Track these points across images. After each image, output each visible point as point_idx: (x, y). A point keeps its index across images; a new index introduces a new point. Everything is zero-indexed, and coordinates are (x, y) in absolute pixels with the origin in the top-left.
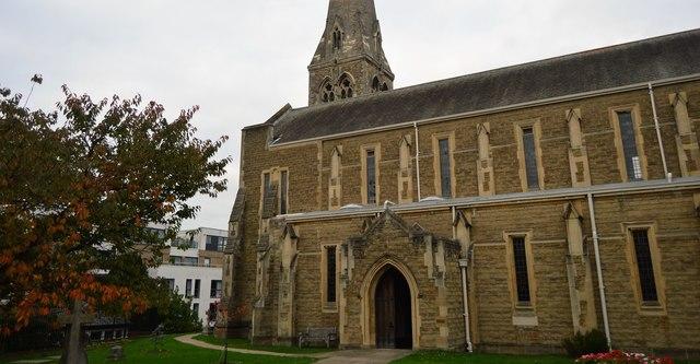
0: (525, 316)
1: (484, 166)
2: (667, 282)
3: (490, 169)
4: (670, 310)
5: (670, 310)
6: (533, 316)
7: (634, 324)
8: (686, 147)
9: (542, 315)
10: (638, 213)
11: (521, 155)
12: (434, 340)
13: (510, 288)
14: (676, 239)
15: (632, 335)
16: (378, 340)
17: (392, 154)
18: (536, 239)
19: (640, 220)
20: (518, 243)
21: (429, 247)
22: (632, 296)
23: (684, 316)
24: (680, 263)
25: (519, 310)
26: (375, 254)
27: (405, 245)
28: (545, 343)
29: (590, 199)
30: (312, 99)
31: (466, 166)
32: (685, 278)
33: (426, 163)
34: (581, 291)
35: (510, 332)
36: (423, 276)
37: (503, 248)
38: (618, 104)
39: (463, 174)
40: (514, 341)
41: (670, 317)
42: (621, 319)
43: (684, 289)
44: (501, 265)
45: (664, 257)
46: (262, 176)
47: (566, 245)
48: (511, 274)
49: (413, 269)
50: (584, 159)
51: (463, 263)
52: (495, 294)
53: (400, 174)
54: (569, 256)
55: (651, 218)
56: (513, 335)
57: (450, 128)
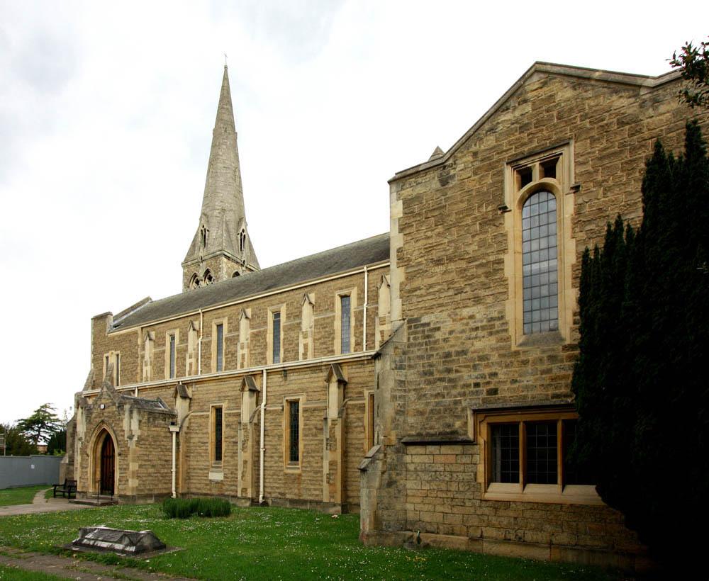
1: (242, 348)
2: (305, 445)
5: (304, 469)
6: (221, 472)
7: (280, 480)
8: (382, 328)
9: (227, 471)
12: (125, 489)
13: (209, 451)
15: (277, 488)
18: (229, 410)
19: (296, 392)
20: (219, 411)
21: (127, 414)
22: (281, 457)
23: (311, 474)
24: (314, 430)
26: (97, 420)
27: (113, 413)
28: (227, 493)
29: (265, 374)
30: (187, 286)
31: (232, 348)
32: (316, 442)
33: (207, 345)
34: (245, 452)
36: (121, 438)
37: (208, 417)
38: (341, 289)
39: (230, 356)
40: (209, 492)
41: (303, 475)
42: (273, 475)
43: (314, 451)
44: (205, 431)
45: (306, 425)
46: (105, 359)
47: (239, 415)
48: (211, 438)
49: (116, 433)
50: (310, 341)
53: (188, 356)
55: (303, 391)
57: (225, 314)
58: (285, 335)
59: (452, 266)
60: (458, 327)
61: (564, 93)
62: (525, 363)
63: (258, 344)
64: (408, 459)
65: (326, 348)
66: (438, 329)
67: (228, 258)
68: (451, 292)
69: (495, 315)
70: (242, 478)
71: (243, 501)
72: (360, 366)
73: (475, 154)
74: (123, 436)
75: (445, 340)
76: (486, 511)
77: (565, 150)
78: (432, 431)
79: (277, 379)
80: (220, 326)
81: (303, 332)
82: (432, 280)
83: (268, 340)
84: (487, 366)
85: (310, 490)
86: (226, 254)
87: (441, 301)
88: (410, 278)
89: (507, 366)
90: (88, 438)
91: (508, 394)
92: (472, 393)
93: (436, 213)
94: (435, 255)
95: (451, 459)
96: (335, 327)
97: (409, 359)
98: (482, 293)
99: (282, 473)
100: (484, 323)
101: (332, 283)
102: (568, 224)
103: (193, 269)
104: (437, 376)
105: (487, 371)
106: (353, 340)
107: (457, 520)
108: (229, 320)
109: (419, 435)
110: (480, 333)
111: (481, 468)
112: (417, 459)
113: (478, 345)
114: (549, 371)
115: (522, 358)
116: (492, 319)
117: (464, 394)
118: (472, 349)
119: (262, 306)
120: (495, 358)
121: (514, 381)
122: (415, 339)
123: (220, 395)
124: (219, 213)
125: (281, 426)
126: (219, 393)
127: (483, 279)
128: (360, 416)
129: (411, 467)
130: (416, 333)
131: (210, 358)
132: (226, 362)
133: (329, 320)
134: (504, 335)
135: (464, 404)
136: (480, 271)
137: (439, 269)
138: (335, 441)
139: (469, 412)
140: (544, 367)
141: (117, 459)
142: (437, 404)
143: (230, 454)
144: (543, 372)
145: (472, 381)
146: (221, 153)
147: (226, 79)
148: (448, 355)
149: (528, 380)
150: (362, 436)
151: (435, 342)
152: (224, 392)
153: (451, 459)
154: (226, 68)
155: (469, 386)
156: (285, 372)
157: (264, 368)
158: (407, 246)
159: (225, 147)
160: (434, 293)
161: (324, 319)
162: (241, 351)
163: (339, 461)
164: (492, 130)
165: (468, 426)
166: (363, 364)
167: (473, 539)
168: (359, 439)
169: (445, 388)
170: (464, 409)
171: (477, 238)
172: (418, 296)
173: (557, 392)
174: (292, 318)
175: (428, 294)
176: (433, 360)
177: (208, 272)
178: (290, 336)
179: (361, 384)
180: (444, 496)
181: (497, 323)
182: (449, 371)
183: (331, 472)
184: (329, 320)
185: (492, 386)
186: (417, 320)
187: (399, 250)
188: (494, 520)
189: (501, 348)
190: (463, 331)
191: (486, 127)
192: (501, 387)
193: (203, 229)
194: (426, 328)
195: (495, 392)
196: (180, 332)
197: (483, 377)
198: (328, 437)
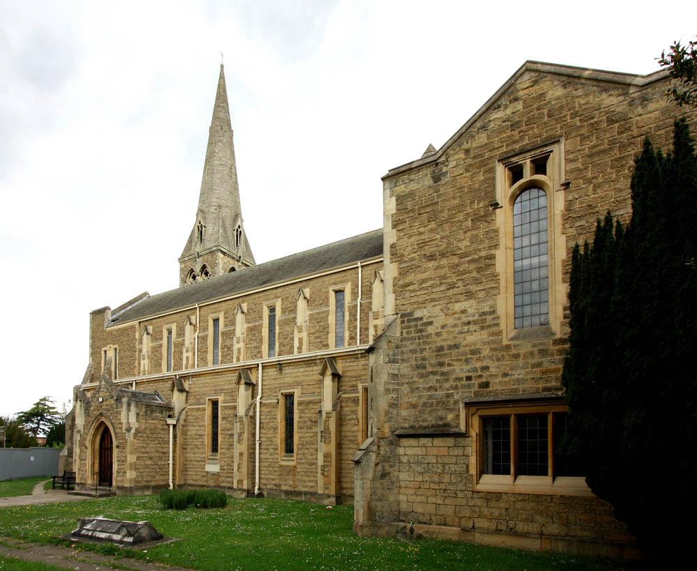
0: (213, 464)
1: (300, 331)
2: (300, 438)
3: (241, 345)
4: (298, 461)
5: (298, 461)
7: (275, 471)
9: (223, 463)
10: (289, 380)
11: (332, 319)
12: (123, 481)
13: (206, 443)
14: (310, 402)
15: (273, 479)
16: (107, 481)
17: (291, 309)
18: (225, 403)
20: (215, 404)
21: (125, 407)
23: (306, 466)
25: (211, 459)
26: (95, 412)
27: (112, 405)
28: (222, 485)
29: (260, 368)
31: (228, 342)
32: (311, 435)
33: (203, 339)
34: (241, 444)
35: (203, 476)
37: (204, 410)
39: (226, 350)
40: (205, 484)
41: (298, 466)
42: (268, 467)
43: (308, 444)
46: (103, 353)
47: (235, 408)
50: (304, 335)
51: (171, 421)
52: (196, 446)
53: (184, 350)
54: (236, 416)
55: (298, 384)
56: (205, 479)
57: (348, 278)
58: (280, 329)
59: (444, 261)
60: (451, 321)
61: (555, 92)
62: (516, 356)
63: (254, 338)
64: (401, 451)
65: (321, 342)
66: (431, 323)
67: (224, 253)
68: (443, 287)
69: (487, 309)
70: (238, 470)
71: (239, 492)
72: (354, 360)
73: (467, 151)
74: (121, 428)
75: (438, 334)
76: (478, 502)
77: (555, 148)
78: (425, 424)
79: (272, 372)
80: (216, 321)
81: (298, 327)
82: (425, 276)
83: (263, 334)
84: (478, 360)
85: (304, 482)
86: (222, 249)
87: (433, 296)
88: (403, 273)
89: (498, 360)
90: (86, 430)
91: (499, 388)
92: (464, 386)
93: (429, 209)
94: (428, 250)
95: (444, 451)
96: (330, 322)
97: (402, 352)
98: (474, 288)
99: (277, 465)
100: (476, 318)
101: (327, 278)
102: (558, 220)
103: (190, 265)
104: (429, 369)
105: (478, 365)
106: (347, 335)
107: (449, 511)
108: (225, 314)
109: (412, 427)
110: (472, 327)
111: (473, 461)
112: (410, 451)
113: (470, 339)
114: (539, 365)
115: (514, 351)
116: (484, 314)
117: (456, 388)
118: (464, 343)
119: (257, 301)
120: (486, 352)
121: (505, 375)
122: (408, 333)
123: (216, 388)
124: (216, 209)
125: (276, 419)
126: (215, 386)
127: (475, 274)
128: (354, 409)
129: (404, 459)
130: (409, 327)
131: (206, 352)
132: (222, 356)
133: (324, 315)
134: (495, 329)
135: (456, 397)
136: (472, 266)
137: (431, 264)
138: (330, 433)
139: (461, 405)
140: (535, 361)
141: (115, 451)
142: (430, 397)
143: (226, 446)
144: (534, 366)
145: (464, 375)
146: (217, 151)
147: (222, 77)
148: (440, 349)
149: (519, 374)
150: (355, 428)
151: (428, 336)
152: (220, 385)
153: (444, 451)
154: (222, 67)
155: (461, 379)
156: (280, 366)
157: (259, 362)
158: (400, 242)
159: (221, 144)
160: (426, 288)
161: (318, 313)
162: (237, 344)
163: (334, 453)
164: (484, 127)
165: (460, 419)
166: (357, 358)
167: (464, 530)
168: (353, 432)
169: (438, 381)
170: (456, 402)
171: (469, 234)
172: (411, 291)
173: (548, 385)
174: (287, 313)
175: (421, 289)
176: (426, 354)
177: (204, 267)
178: (286, 330)
179: (354, 377)
180: (437, 487)
181: (489, 317)
182: (441, 364)
183: (326, 463)
184: (324, 315)
185: (484, 380)
186: (411, 314)
187: (393, 246)
188: (486, 511)
189: (493, 342)
190: (455, 326)
191: (478, 124)
192: (492, 381)
193: (200, 225)
194: (419, 323)
195: (486, 385)
196: (177, 326)
197: (475, 370)
198: (323, 430)
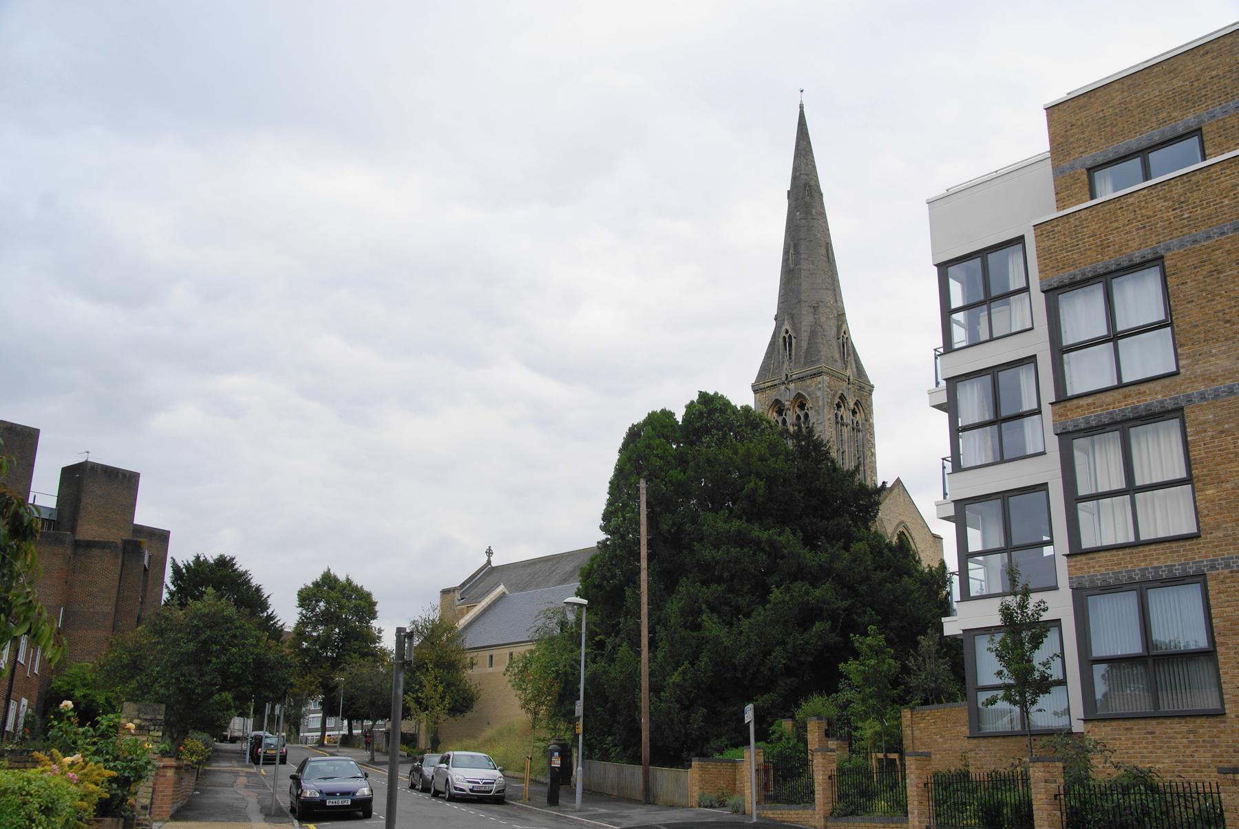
154: (801, 107)
193: (787, 336)
